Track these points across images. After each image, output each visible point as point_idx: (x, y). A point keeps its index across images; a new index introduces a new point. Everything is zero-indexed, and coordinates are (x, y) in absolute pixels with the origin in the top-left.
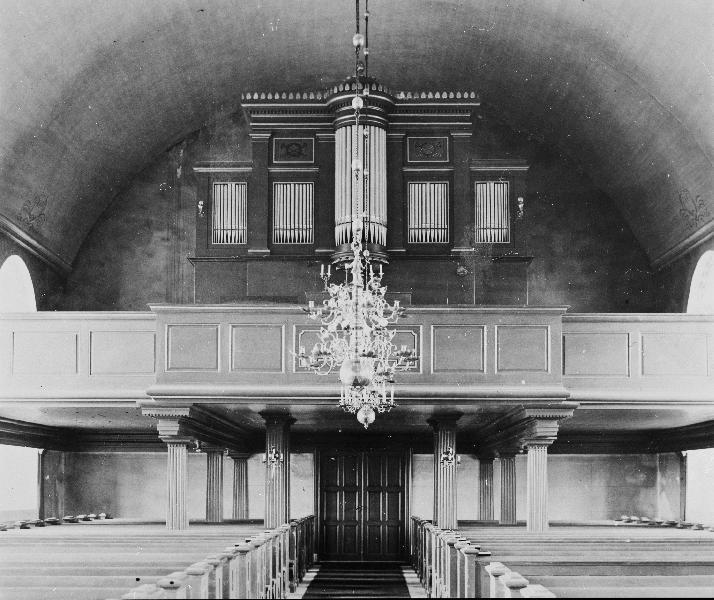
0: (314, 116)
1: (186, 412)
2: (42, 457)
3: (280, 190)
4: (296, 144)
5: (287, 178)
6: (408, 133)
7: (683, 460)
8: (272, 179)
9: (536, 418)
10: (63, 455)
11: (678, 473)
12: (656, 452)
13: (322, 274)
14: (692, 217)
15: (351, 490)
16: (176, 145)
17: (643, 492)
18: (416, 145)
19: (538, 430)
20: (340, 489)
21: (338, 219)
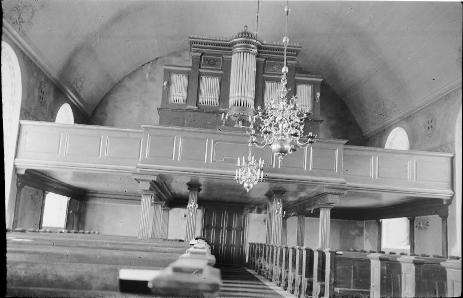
0: (222, 47)
1: (155, 178)
2: (70, 203)
3: (204, 80)
4: (213, 60)
5: (208, 75)
6: (266, 59)
7: (380, 224)
8: (200, 74)
9: (329, 193)
10: (79, 203)
11: (377, 230)
12: (364, 220)
13: (222, 117)
14: (388, 112)
15: (218, 229)
16: (147, 63)
17: (357, 238)
18: (271, 65)
19: (329, 200)
20: (213, 228)
21: (231, 95)
